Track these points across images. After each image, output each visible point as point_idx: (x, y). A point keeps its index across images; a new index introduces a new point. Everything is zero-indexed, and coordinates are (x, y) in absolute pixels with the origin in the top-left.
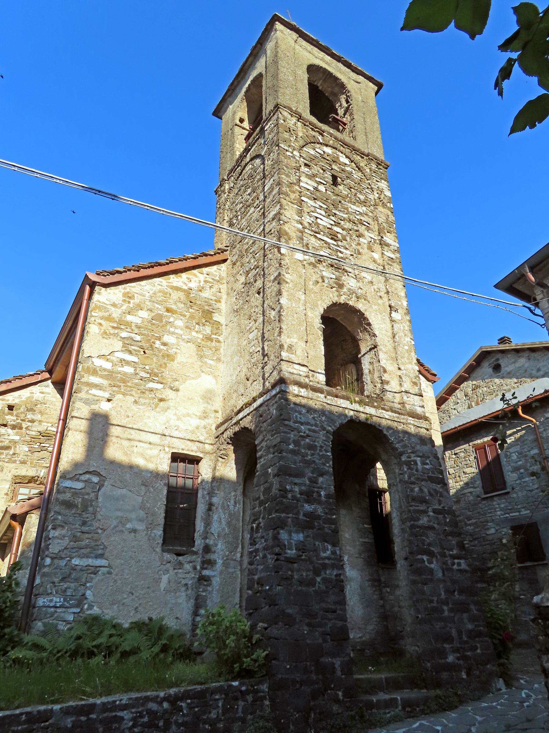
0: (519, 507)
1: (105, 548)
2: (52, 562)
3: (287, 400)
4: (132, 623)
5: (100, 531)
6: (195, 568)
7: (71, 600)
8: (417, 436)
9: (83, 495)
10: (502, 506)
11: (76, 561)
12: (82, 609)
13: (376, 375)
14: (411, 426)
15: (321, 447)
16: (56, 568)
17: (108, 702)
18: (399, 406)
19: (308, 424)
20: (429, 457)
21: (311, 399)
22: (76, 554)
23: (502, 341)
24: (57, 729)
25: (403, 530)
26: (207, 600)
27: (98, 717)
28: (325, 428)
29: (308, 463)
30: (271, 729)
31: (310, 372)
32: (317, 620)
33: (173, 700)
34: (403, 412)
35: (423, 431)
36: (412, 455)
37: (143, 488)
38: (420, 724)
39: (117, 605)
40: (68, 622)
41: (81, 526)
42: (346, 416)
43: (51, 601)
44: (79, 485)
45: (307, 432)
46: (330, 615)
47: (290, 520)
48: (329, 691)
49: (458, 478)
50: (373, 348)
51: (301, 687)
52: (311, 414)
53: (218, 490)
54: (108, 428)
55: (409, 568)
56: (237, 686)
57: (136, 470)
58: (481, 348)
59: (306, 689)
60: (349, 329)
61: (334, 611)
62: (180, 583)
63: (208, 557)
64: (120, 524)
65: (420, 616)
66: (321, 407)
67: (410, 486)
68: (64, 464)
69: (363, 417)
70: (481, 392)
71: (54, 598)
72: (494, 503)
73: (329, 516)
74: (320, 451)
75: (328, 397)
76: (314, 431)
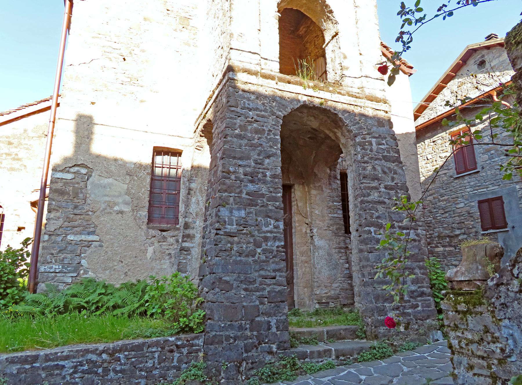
0: (487, 184)
1: (96, 226)
2: (50, 238)
3: (235, 87)
4: (122, 284)
5: (90, 213)
6: (177, 241)
7: (68, 267)
8: (374, 118)
9: (74, 184)
10: (472, 183)
11: (70, 237)
12: (78, 274)
13: (338, 61)
14: (369, 109)
15: (270, 131)
16: (53, 243)
17: (51, 354)
18: (358, 91)
19: (257, 109)
20: (385, 138)
21: (262, 86)
22: (71, 231)
23: (489, 38)
24: (4, 374)
25: (356, 206)
26: (187, 266)
27: (41, 365)
28: (276, 113)
29: (254, 147)
30: (202, 377)
31: (262, 59)
32: (255, 286)
33: (112, 353)
34: (361, 96)
35: (381, 114)
36: (368, 136)
37: (128, 177)
38: (349, 372)
39: (109, 271)
40: (68, 284)
41: (74, 209)
42: (299, 101)
43: (51, 268)
44: (69, 176)
45: (255, 117)
46: (268, 281)
47: (232, 199)
48: (263, 345)
49: (435, 162)
50: (335, 36)
51: (235, 341)
52: (260, 101)
53: (196, 177)
54: (93, 127)
55: (358, 238)
56: (173, 341)
57: (120, 162)
58: (468, 47)
59: (241, 343)
60: (314, 20)
61: (274, 278)
62: (164, 253)
63: (187, 232)
64: (108, 208)
65: (364, 279)
66: (272, 93)
67: (363, 164)
68: (56, 160)
69: (317, 101)
70: (465, 87)
71: (54, 266)
72: (465, 182)
73: (274, 195)
74: (268, 134)
75: (279, 83)
76: (263, 117)
